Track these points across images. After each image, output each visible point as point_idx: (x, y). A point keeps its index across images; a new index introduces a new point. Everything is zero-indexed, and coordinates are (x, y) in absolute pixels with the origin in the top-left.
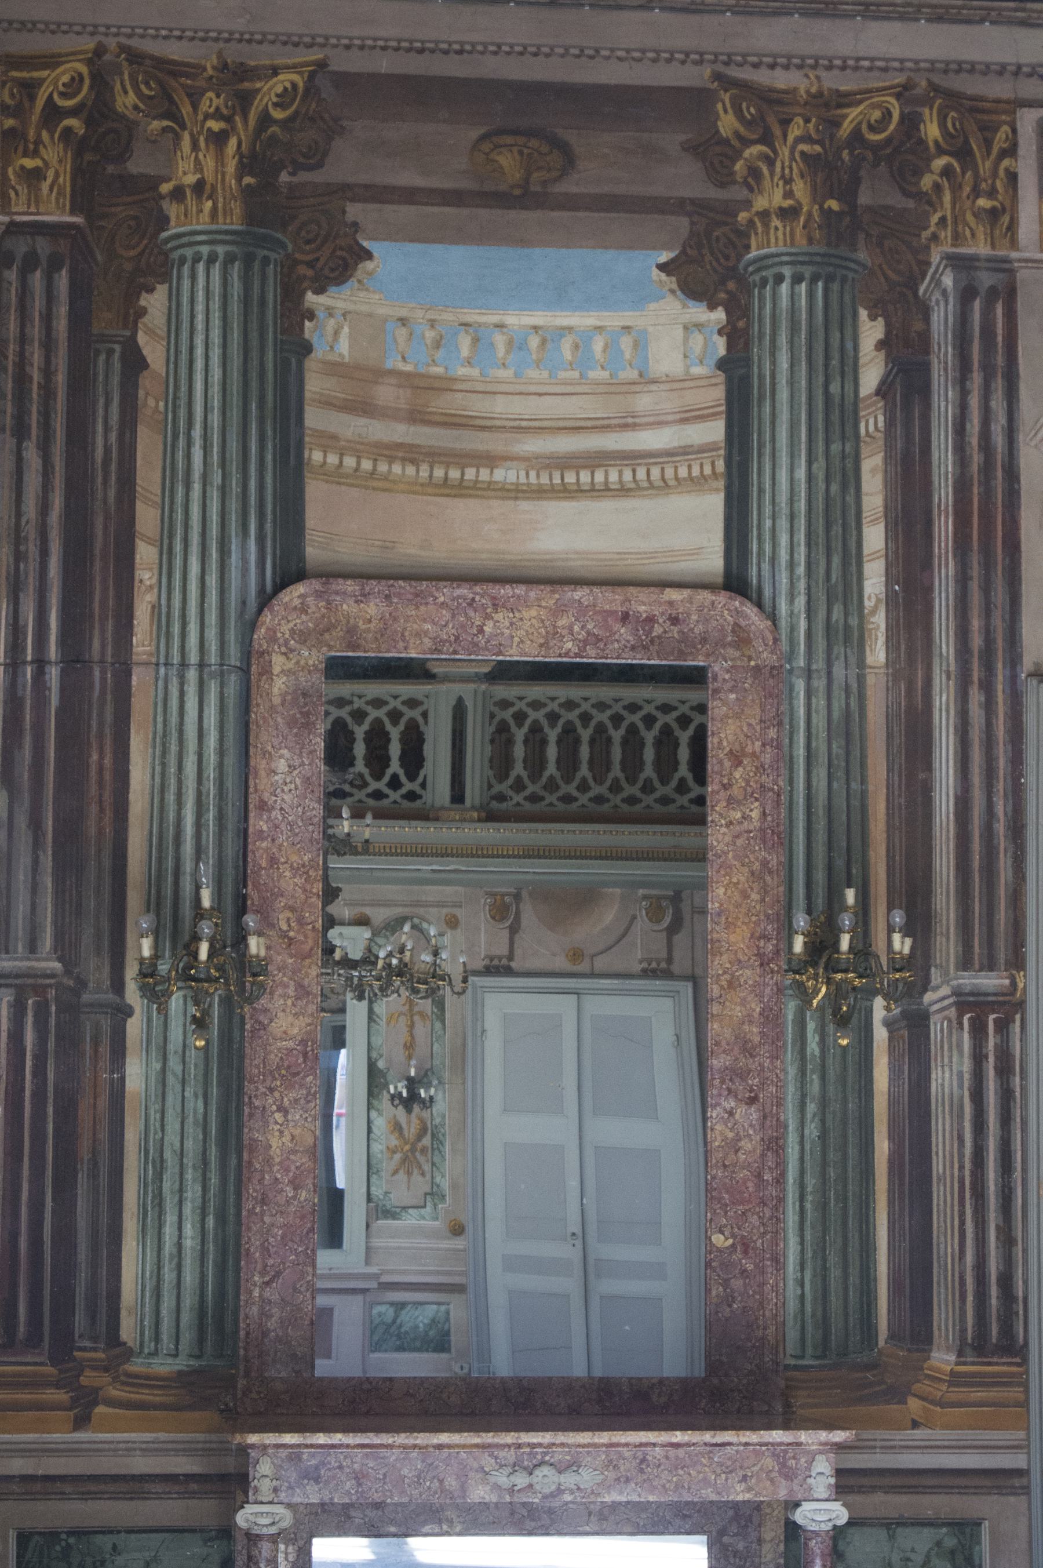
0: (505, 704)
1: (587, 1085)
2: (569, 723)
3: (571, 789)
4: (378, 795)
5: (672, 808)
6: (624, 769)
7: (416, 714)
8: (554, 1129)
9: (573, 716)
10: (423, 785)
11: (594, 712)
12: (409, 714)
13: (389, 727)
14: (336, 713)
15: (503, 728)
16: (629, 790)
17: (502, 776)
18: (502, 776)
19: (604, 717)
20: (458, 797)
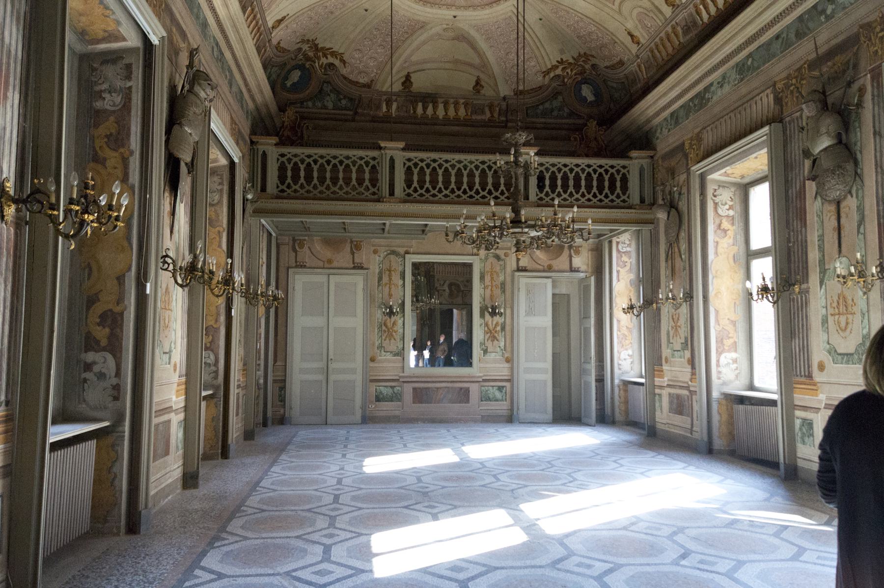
0: (409, 160)
1: (326, 307)
2: (577, 172)
3: (614, 197)
4: (577, 200)
5: (324, 195)
6: (609, 189)
7: (625, 171)
8: (337, 321)
9: (461, 166)
10: (628, 197)
11: (609, 169)
12: (623, 171)
13: (287, 164)
14: (408, 164)
15: (409, 168)
16: (588, 196)
17: (409, 187)
18: (409, 187)
19: (472, 166)
20: (392, 193)
